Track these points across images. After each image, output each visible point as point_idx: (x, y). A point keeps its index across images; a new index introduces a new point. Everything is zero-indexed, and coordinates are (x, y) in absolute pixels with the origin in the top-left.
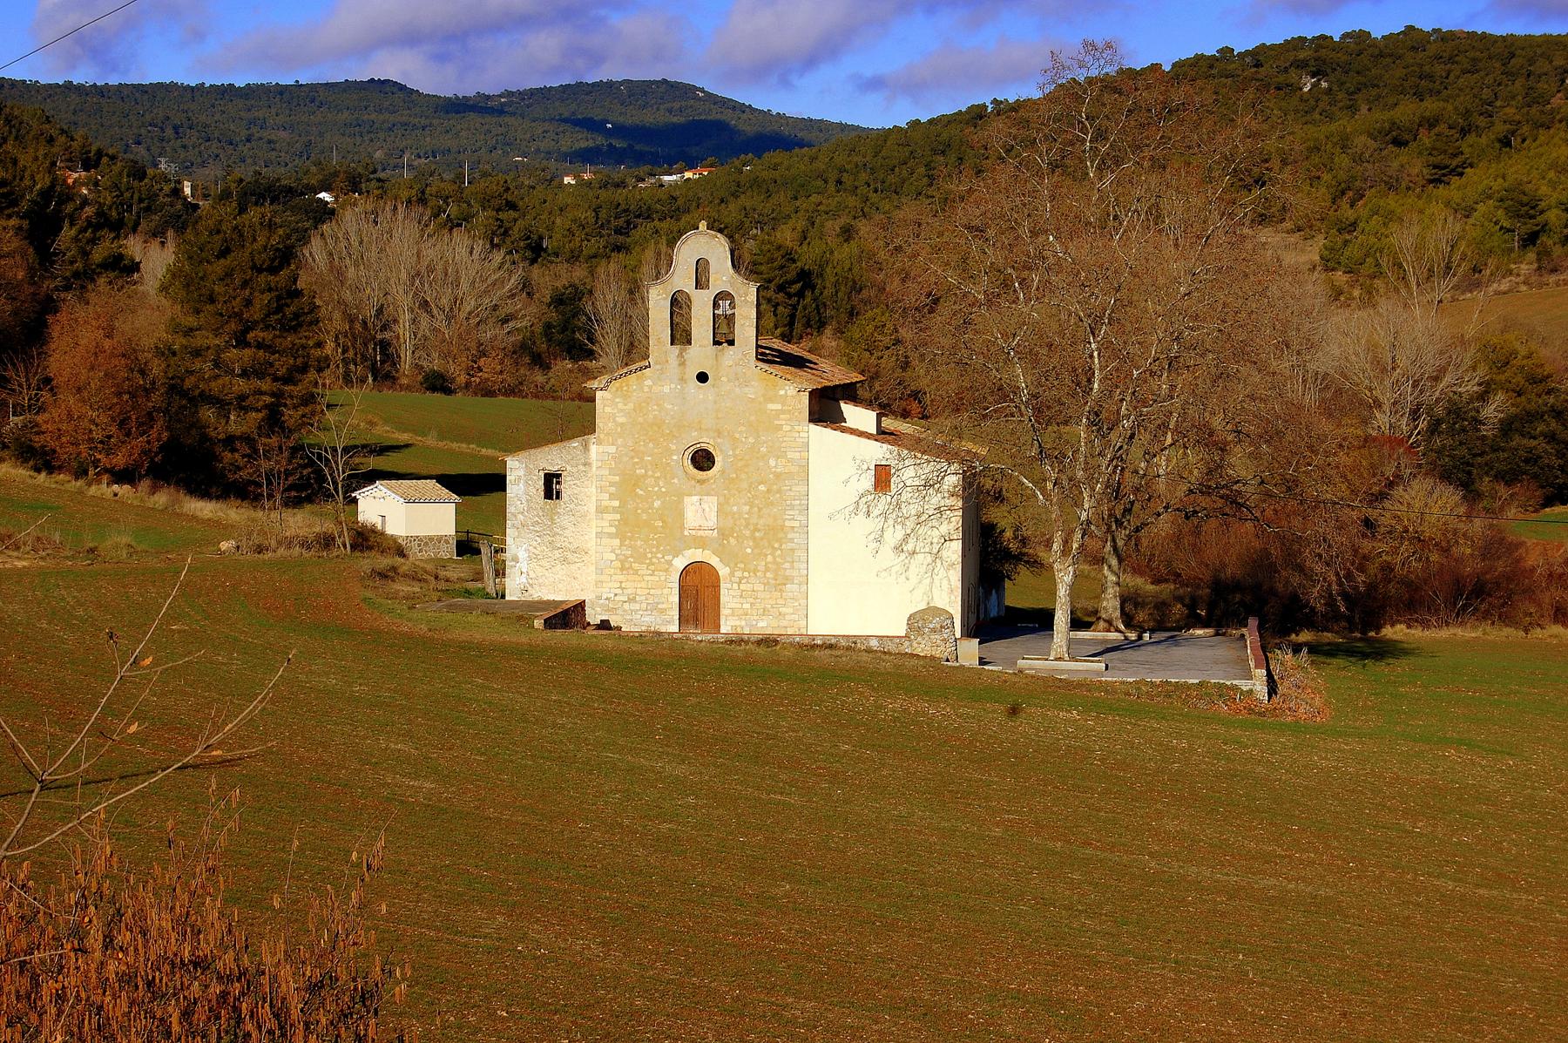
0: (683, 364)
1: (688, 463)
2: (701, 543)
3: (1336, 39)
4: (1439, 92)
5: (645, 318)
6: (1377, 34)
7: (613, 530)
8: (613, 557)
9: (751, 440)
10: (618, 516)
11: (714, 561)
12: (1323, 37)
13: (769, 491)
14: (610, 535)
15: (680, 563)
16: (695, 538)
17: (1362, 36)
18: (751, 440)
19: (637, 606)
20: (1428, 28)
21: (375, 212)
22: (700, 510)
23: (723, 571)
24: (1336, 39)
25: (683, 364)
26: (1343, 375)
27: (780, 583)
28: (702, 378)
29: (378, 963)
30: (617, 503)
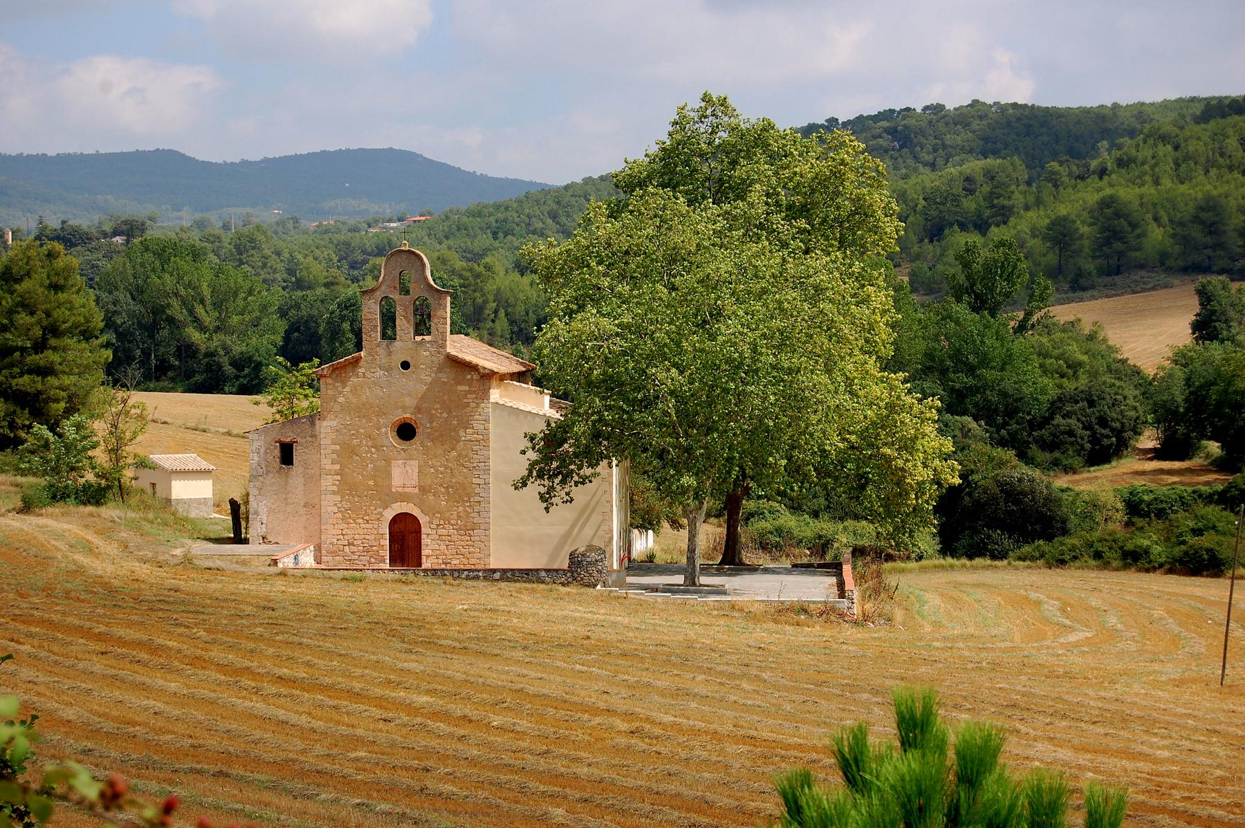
0: (390, 354)
1: (406, 445)
2: (404, 498)
3: (919, 110)
4: (1000, 151)
5: (713, 575)
6: (950, 105)
7: (335, 488)
8: (336, 510)
9: (445, 415)
10: (339, 478)
11: (416, 512)
12: (908, 109)
13: (459, 455)
14: (334, 493)
15: (389, 514)
16: (401, 494)
17: (938, 109)
18: (445, 415)
19: (355, 549)
20: (990, 101)
21: (966, 265)
22: (405, 471)
23: (423, 519)
24: (919, 110)
25: (390, 354)
26: (511, 290)
27: (468, 529)
28: (405, 365)
29: (168, 708)
30: (337, 467)
